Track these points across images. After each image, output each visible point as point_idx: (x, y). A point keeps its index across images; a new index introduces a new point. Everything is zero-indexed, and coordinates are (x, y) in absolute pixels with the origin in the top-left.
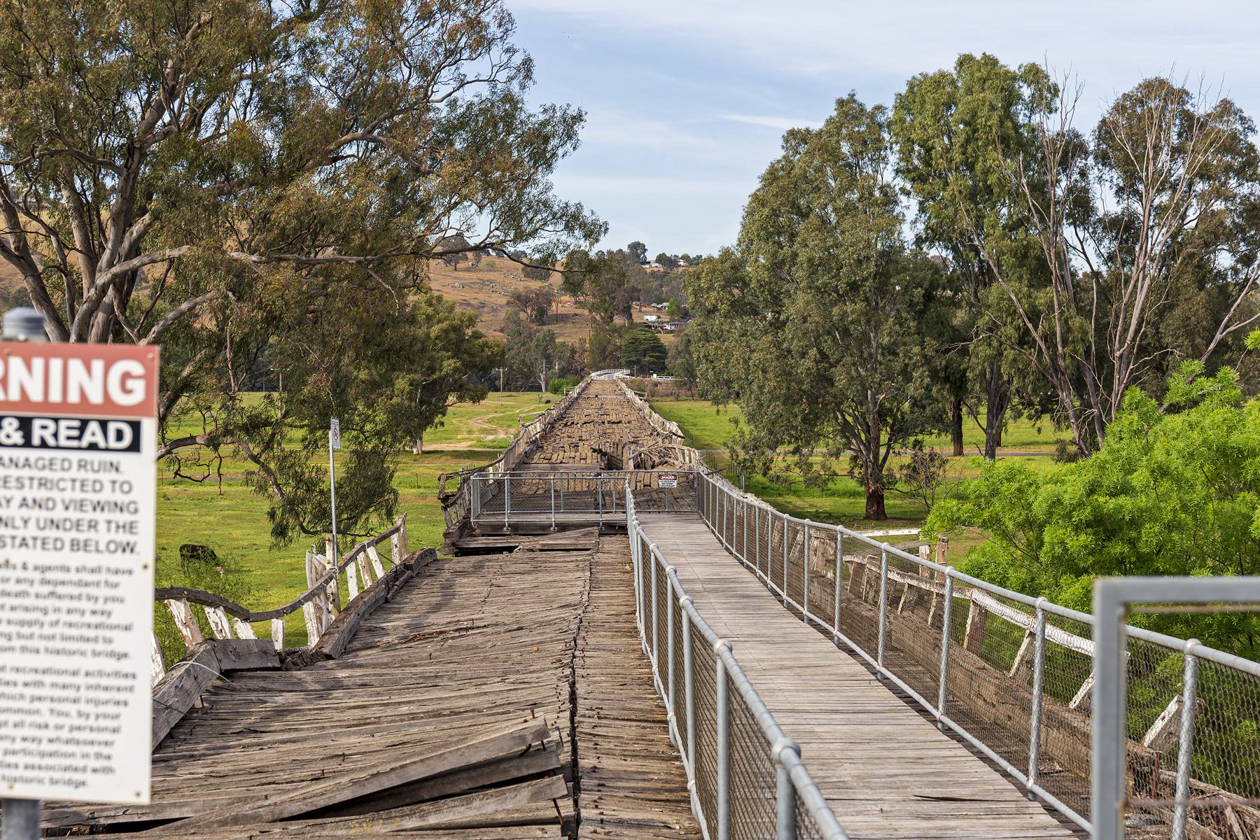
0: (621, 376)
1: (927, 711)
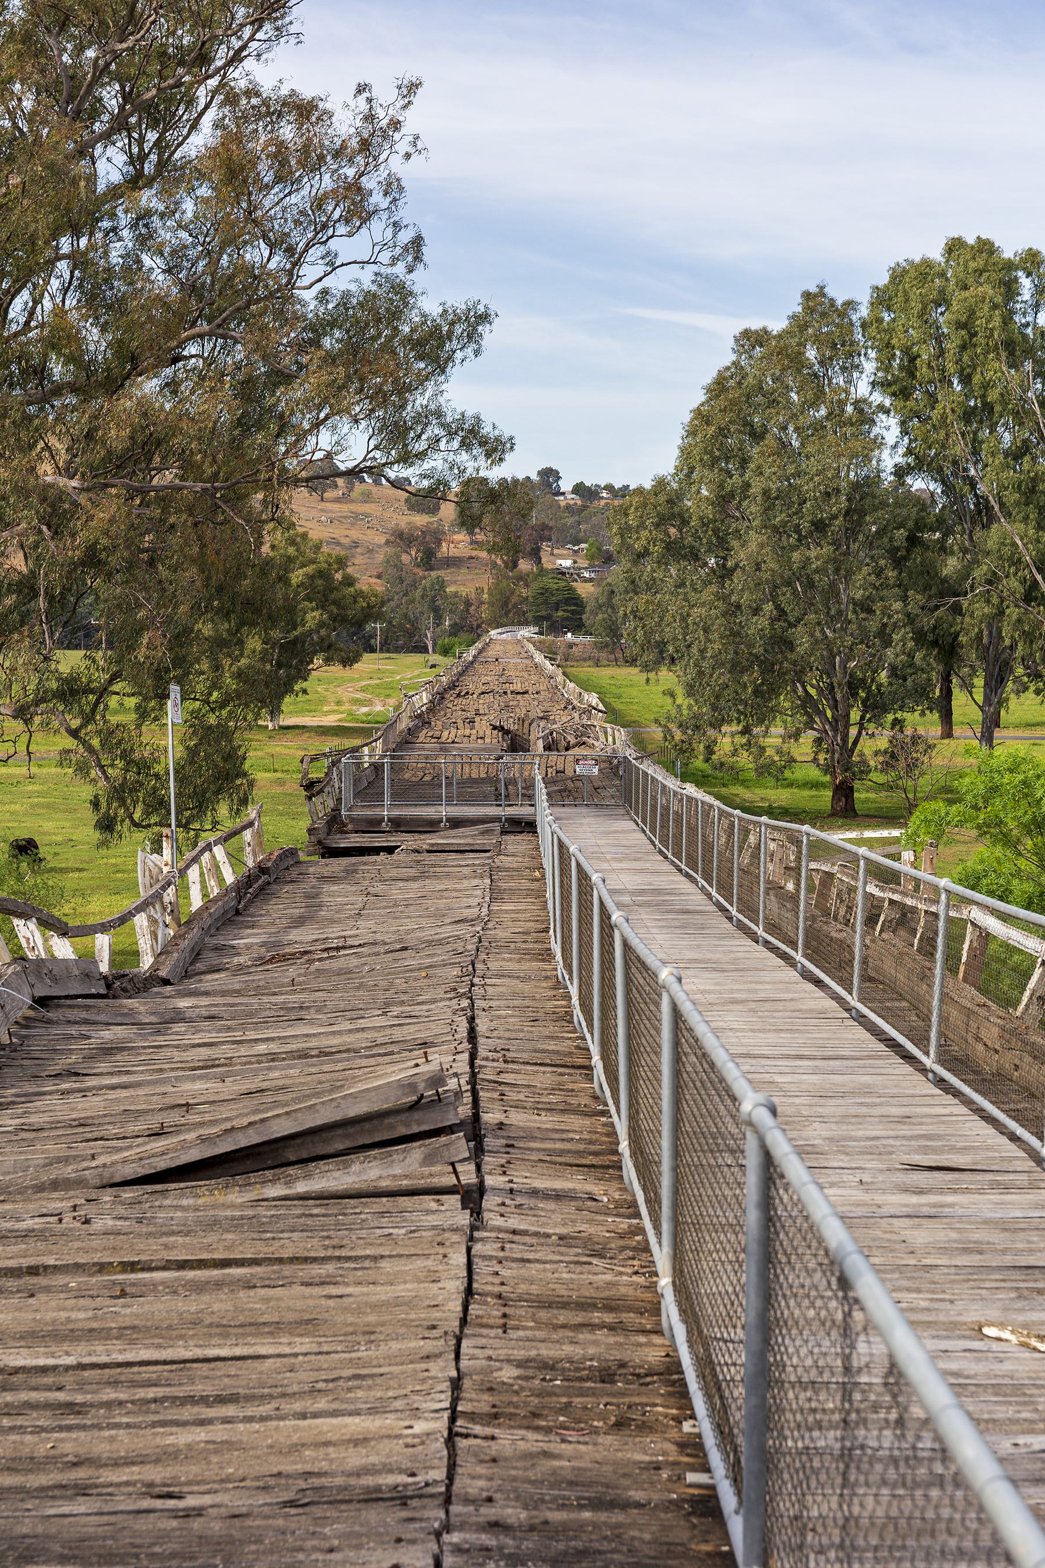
0: (527, 635)
1: (915, 1058)
